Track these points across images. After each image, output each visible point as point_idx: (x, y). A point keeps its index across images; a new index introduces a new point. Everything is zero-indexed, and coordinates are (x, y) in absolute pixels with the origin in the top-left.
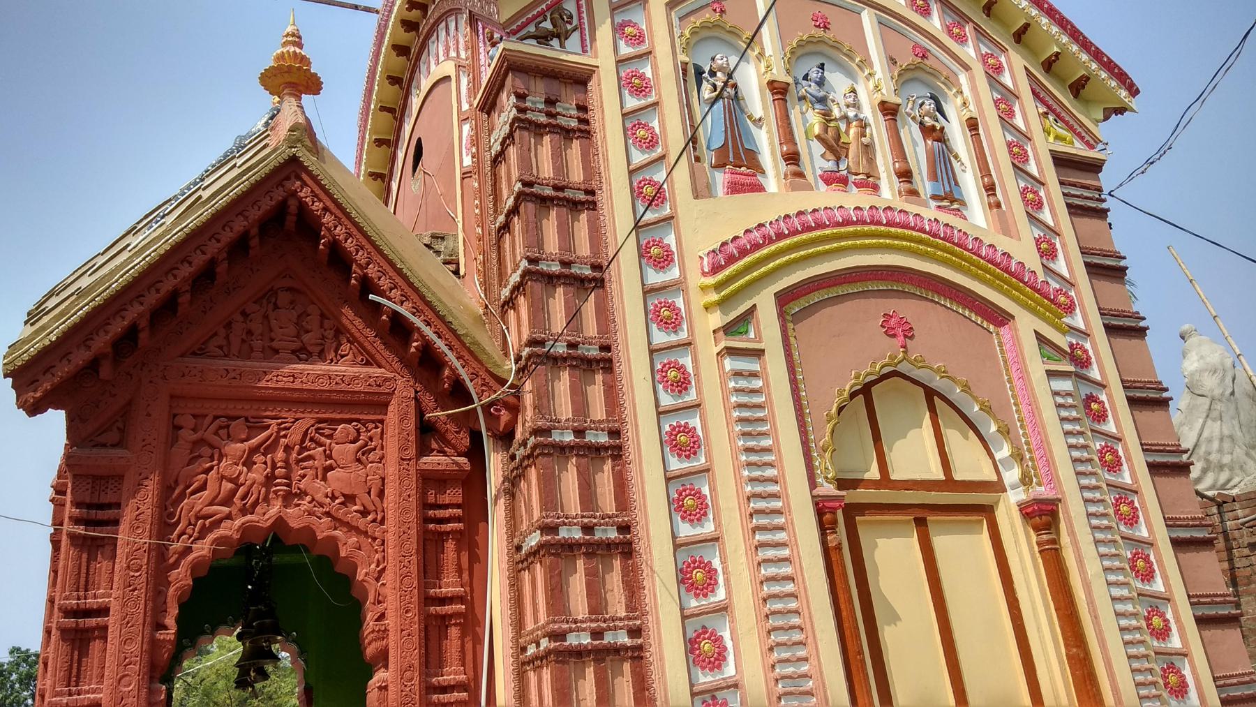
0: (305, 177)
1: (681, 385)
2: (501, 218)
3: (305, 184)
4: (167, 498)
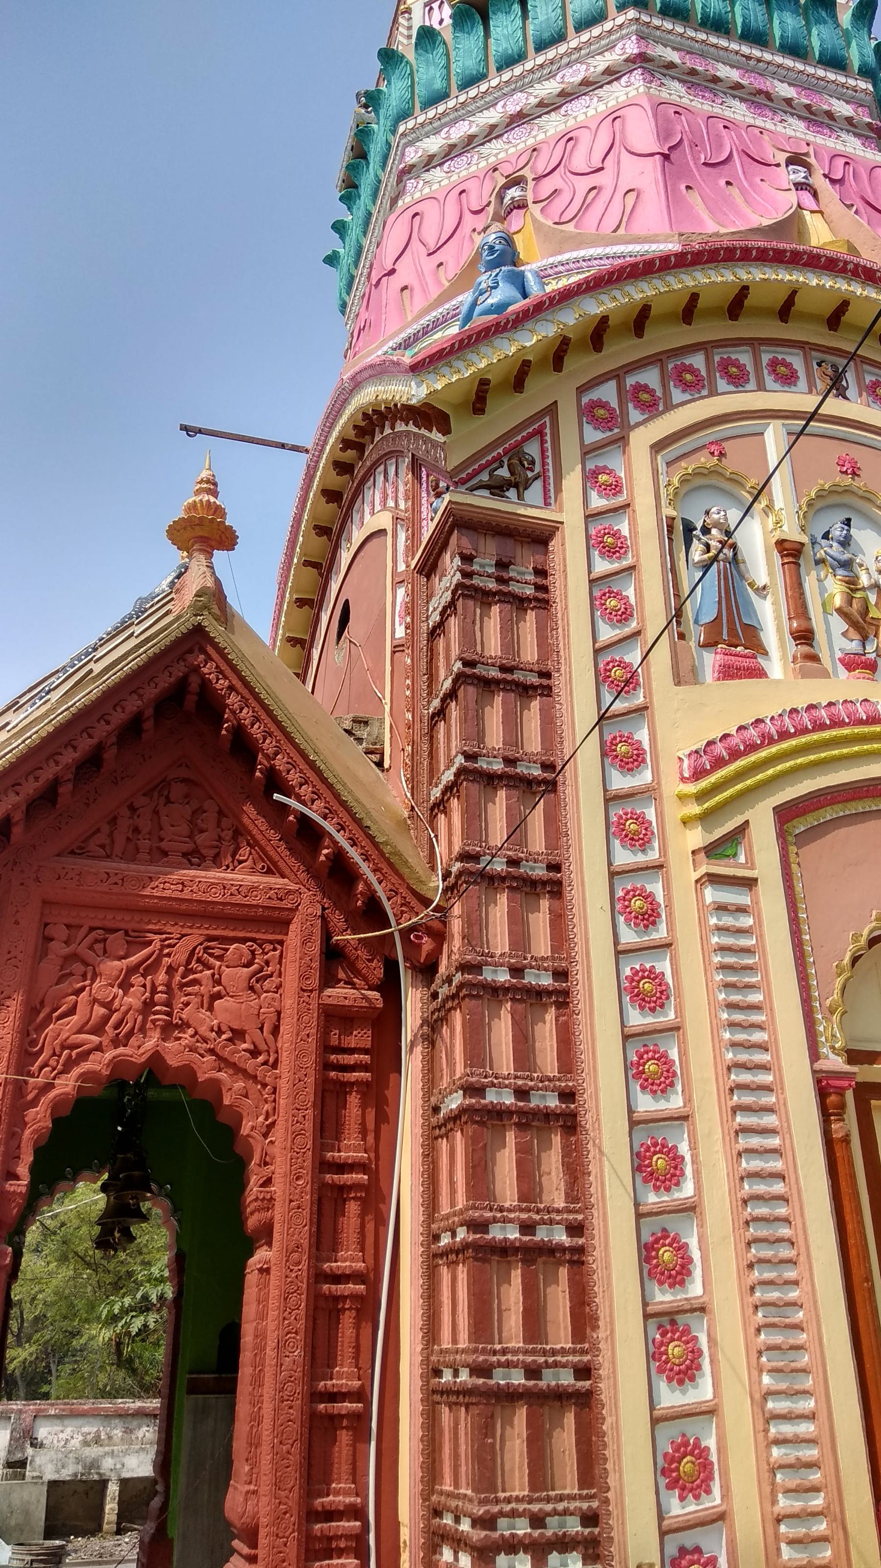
0: (210, 650)
3: (209, 658)
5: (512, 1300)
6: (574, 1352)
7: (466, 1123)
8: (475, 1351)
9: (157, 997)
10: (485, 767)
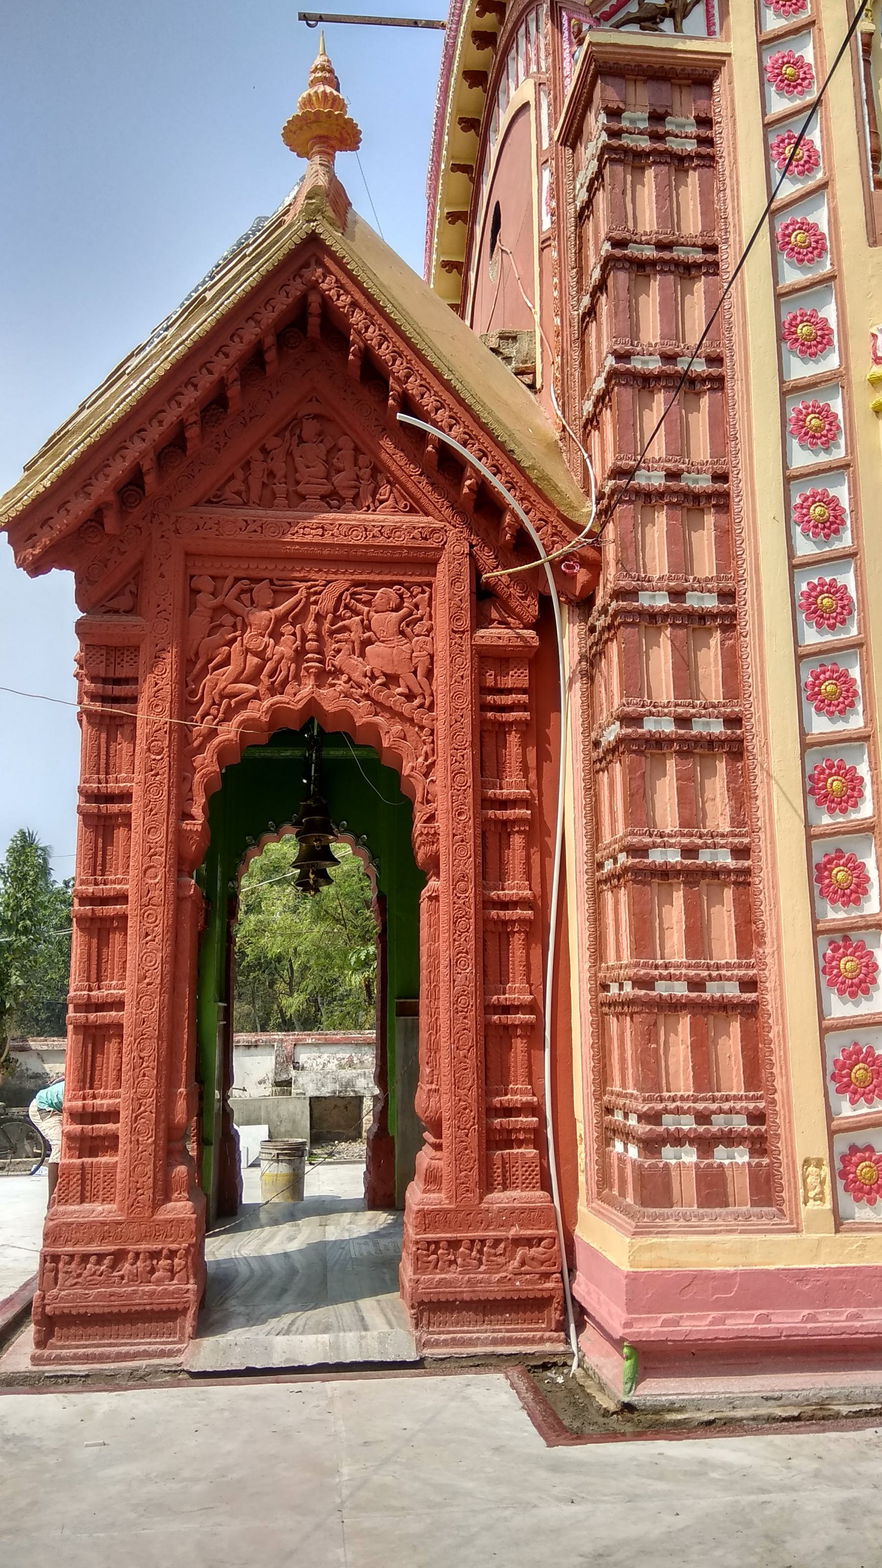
0: (328, 261)
1: (830, 526)
2: (586, 300)
3: (328, 272)
4: (188, 674)
5: (675, 919)
6: (740, 966)
7: (623, 753)
8: (637, 965)
9: (308, 645)
10: (639, 367)
